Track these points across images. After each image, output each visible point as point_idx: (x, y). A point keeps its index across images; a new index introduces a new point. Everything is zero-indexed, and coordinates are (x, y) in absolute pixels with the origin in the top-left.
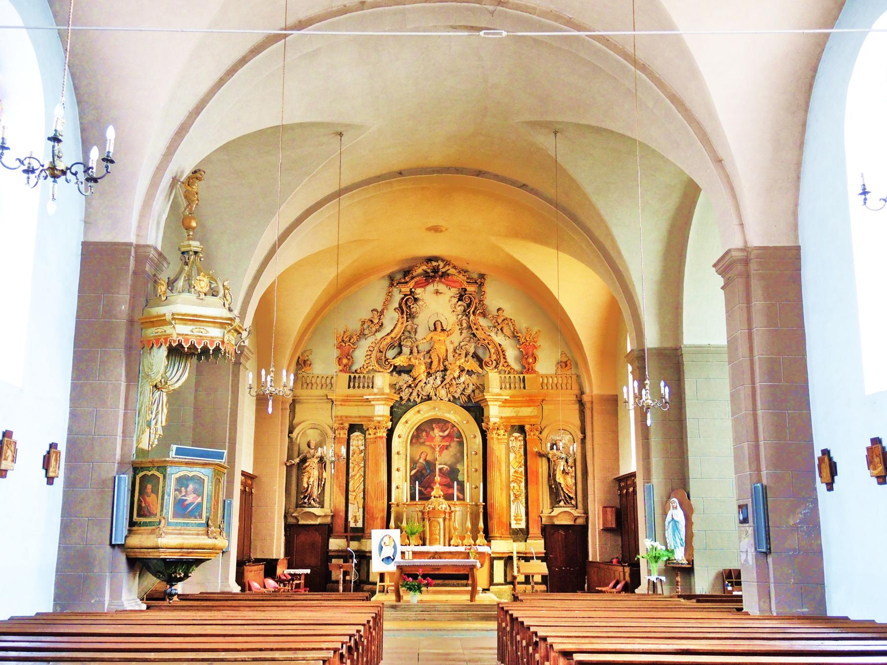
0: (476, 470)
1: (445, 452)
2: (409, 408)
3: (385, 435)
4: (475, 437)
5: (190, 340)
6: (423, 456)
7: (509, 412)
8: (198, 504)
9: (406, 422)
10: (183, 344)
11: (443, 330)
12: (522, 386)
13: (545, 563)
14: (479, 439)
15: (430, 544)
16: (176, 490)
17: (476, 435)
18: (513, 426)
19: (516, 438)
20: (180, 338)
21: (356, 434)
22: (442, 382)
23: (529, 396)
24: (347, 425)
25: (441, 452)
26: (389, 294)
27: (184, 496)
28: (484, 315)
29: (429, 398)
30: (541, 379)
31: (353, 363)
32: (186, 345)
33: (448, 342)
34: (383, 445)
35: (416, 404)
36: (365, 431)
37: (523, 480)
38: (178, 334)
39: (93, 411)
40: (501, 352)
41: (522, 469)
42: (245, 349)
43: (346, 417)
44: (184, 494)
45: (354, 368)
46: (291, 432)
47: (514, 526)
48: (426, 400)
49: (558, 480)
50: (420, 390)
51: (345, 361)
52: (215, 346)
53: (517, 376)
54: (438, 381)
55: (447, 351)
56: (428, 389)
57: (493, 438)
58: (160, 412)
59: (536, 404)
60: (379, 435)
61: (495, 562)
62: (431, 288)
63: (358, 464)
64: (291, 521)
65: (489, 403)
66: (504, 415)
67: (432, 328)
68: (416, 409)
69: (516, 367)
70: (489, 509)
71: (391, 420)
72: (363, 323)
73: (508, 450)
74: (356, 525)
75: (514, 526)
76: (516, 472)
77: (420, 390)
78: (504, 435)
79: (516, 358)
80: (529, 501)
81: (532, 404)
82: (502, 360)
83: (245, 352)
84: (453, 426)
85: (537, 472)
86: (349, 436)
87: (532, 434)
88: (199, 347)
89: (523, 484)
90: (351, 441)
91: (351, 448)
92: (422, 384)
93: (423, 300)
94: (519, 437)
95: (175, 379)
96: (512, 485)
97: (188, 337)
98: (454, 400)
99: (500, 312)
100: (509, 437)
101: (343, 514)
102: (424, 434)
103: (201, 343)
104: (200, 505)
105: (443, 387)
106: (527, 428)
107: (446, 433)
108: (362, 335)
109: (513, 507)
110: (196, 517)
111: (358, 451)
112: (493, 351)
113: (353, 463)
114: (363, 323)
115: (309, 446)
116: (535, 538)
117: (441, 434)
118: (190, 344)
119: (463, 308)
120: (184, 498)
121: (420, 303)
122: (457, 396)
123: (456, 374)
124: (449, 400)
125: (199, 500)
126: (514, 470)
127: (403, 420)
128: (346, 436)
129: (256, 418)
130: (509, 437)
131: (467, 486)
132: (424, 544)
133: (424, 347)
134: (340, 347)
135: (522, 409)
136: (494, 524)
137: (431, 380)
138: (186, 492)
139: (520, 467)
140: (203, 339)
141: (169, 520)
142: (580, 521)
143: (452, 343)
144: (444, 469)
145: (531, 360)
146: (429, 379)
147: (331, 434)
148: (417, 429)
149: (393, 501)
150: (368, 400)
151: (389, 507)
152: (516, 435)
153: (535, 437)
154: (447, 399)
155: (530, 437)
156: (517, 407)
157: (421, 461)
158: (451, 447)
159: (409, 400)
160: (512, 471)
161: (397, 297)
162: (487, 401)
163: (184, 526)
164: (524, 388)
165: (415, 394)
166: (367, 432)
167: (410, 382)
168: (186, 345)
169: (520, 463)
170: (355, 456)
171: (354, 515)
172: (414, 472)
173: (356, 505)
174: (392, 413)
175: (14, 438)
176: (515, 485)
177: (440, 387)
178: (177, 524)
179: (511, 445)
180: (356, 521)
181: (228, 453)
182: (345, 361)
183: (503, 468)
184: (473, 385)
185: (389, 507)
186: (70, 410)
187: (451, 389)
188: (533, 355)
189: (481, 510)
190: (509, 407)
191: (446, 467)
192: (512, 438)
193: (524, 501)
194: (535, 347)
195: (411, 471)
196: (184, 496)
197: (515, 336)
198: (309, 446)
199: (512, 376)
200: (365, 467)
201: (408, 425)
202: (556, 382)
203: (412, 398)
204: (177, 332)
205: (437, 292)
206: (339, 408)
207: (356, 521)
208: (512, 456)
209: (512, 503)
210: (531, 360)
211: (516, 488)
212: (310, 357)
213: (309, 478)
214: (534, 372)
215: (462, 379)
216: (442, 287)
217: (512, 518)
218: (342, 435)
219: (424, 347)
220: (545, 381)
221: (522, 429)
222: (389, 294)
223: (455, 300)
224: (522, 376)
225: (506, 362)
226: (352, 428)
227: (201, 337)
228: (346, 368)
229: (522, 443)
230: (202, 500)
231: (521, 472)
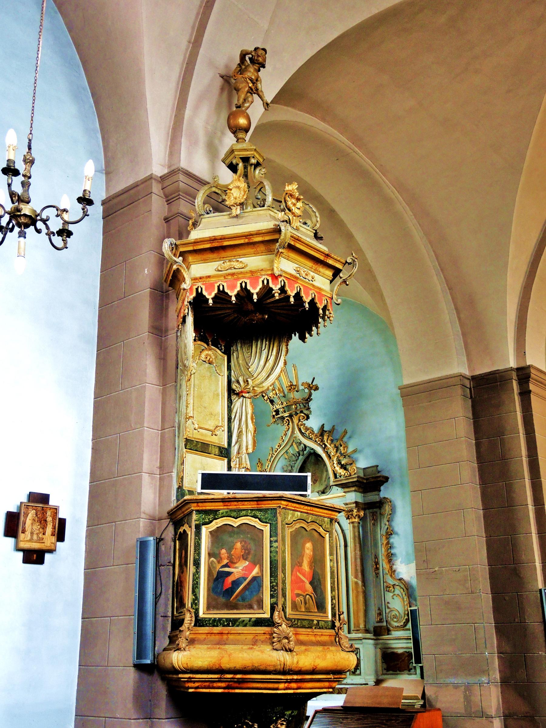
5: (216, 285)
8: (254, 579)
10: (205, 293)
13: (12, 190)
16: (210, 555)
20: (200, 284)
27: (226, 566)
32: (210, 294)
38: (195, 279)
39: (117, 437)
42: (532, 371)
44: (225, 562)
52: (260, 286)
58: (244, 432)
83: (532, 375)
88: (233, 293)
95: (264, 374)
97: (212, 280)
103: (235, 287)
104: (257, 581)
110: (251, 607)
118: (216, 291)
120: (227, 569)
125: (255, 572)
138: (230, 557)
140: (238, 279)
141: (201, 615)
163: (228, 625)
168: (210, 294)
175: (52, 502)
178: (215, 623)
181: (312, 476)
186: (93, 443)
196: (226, 566)
204: (193, 276)
227: (233, 274)
230: (262, 570)
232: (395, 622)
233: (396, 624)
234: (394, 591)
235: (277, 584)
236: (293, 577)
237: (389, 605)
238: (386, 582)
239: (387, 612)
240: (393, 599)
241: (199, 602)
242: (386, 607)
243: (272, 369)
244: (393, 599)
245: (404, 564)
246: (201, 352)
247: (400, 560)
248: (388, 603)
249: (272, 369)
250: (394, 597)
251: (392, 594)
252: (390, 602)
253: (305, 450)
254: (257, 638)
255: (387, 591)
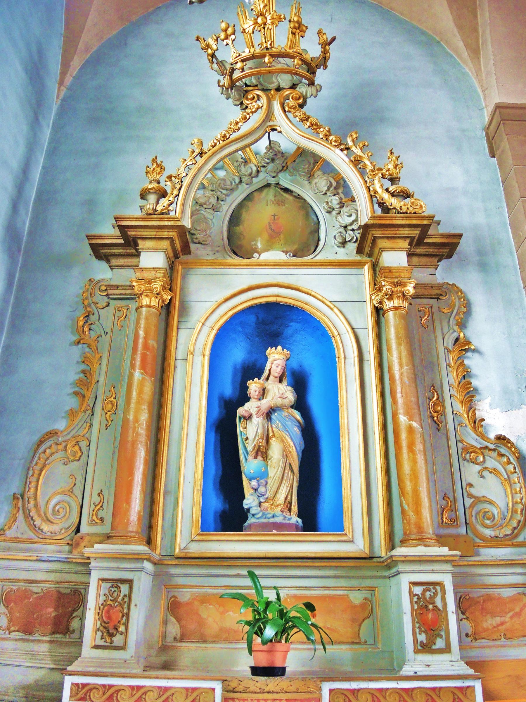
232: (487, 527)
233: (488, 532)
234: (484, 461)
235: (258, 440)
236: (119, 542)
237: (473, 491)
238: (461, 441)
239: (467, 505)
240: (482, 477)
241: (444, 407)
242: (465, 494)
243: (33, 458)
244: (482, 477)
245: (498, 410)
246: (68, 544)
247: (488, 401)
248: (470, 485)
249: (33, 458)
250: (486, 473)
251: (478, 468)
252: (473, 484)
253: (257, 176)
254: (410, 274)
255: (465, 459)
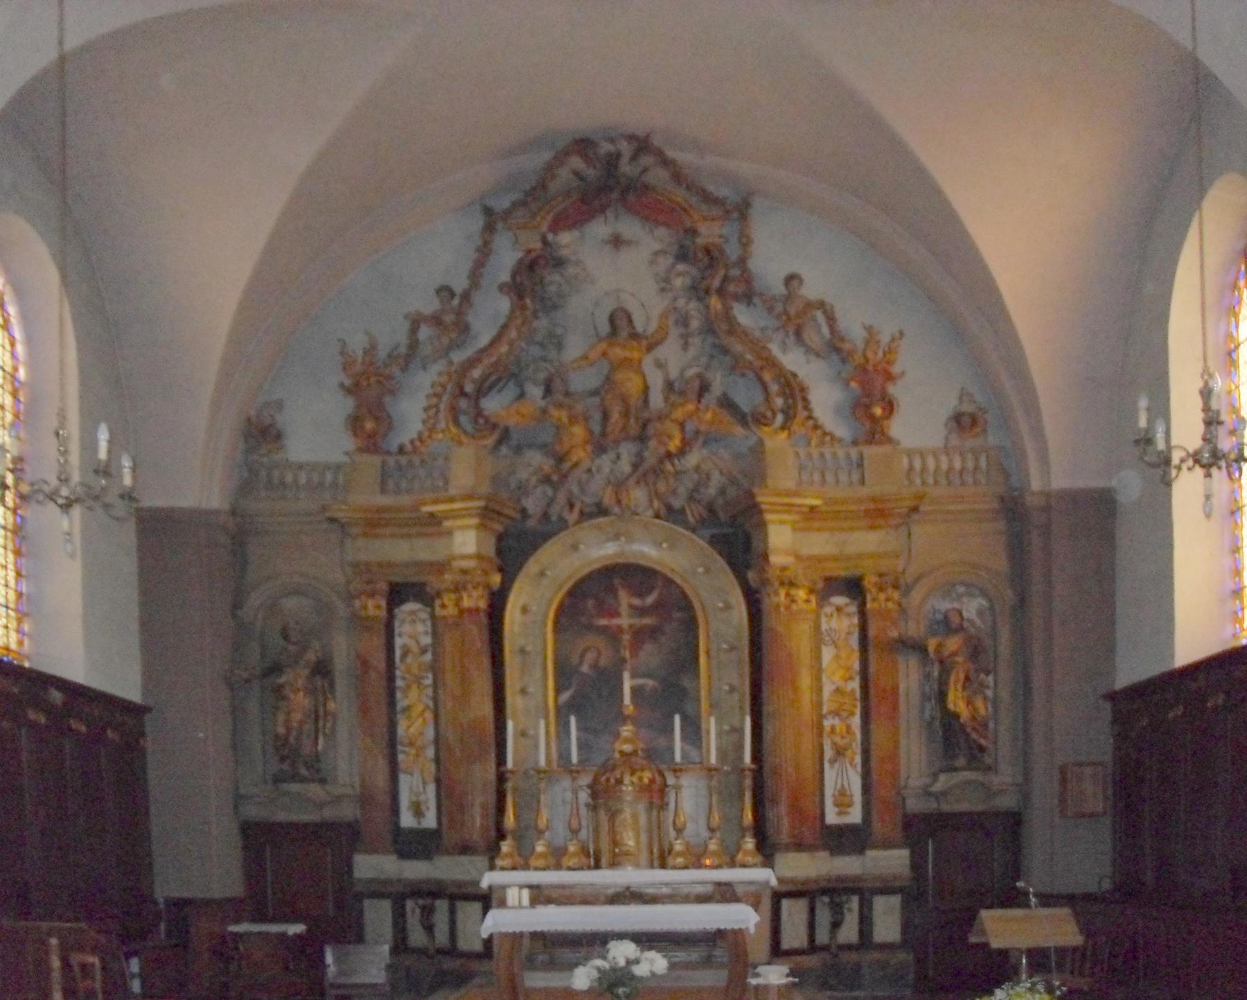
0: (732, 689)
1: (648, 647)
2: (546, 537)
3: (483, 604)
4: (728, 607)
6: (590, 656)
7: (819, 544)
9: (542, 574)
11: (634, 336)
12: (855, 477)
14: (740, 612)
15: (613, 865)
17: (733, 601)
18: (828, 580)
19: (839, 609)
21: (410, 606)
22: (635, 466)
23: (874, 500)
24: (383, 586)
25: (636, 648)
26: (484, 252)
28: (748, 297)
29: (602, 511)
30: (905, 461)
31: (390, 427)
33: (648, 363)
34: (477, 635)
35: (563, 525)
36: (433, 599)
37: (858, 711)
40: (794, 391)
41: (855, 685)
43: (380, 565)
45: (394, 442)
46: (237, 605)
47: (832, 818)
48: (591, 516)
49: (951, 706)
50: (575, 489)
51: (369, 425)
53: (841, 453)
54: (625, 466)
55: (646, 389)
56: (598, 488)
57: (778, 606)
59: (894, 522)
60: (466, 603)
61: (786, 904)
62: (599, 229)
63: (418, 680)
64: (253, 812)
65: (769, 517)
66: (805, 551)
67: (605, 328)
68: (564, 538)
69: (842, 430)
70: (769, 782)
71: (501, 570)
72: (416, 322)
73: (818, 639)
74: (419, 823)
75: (832, 818)
76: (838, 690)
77: (575, 489)
78: (808, 601)
79: (838, 410)
80: (872, 692)
81: (880, 521)
82: (802, 414)
84: (669, 582)
85: (895, 689)
86: (390, 610)
87: (882, 596)
89: (856, 721)
90: (397, 624)
91: (398, 642)
92: (579, 473)
93: (578, 263)
94: (847, 605)
96: (827, 723)
98: (672, 514)
99: (795, 283)
100: (820, 606)
101: (384, 799)
102: (590, 603)
105: (638, 483)
106: (870, 582)
107: (650, 600)
108: (410, 356)
109: (830, 775)
111: (415, 649)
112: (774, 388)
113: (404, 678)
114: (416, 322)
115: (286, 637)
116: (887, 845)
117: (636, 602)
119: (688, 281)
121: (571, 270)
122: (677, 504)
123: (674, 445)
124: (657, 516)
126: (833, 687)
127: (532, 567)
128: (383, 613)
129: (145, 573)
130: (820, 606)
131: (711, 726)
132: (597, 866)
133: (584, 380)
134: (352, 390)
135: (856, 535)
136: (781, 820)
137: (605, 461)
139: (851, 678)
142: (1007, 802)
143: (660, 365)
144: (648, 689)
145: (878, 411)
146: (598, 462)
147: (342, 610)
148: (571, 593)
149: (510, 764)
150: (435, 520)
151: (501, 778)
152: (839, 600)
153: (890, 605)
154: (650, 513)
155: (876, 605)
156: (842, 530)
157: (585, 668)
158: (664, 634)
159: (546, 516)
160: (828, 689)
161: (506, 258)
162: (761, 512)
164: (862, 482)
165: (561, 498)
166: (438, 602)
167: (547, 468)
169: (849, 669)
170: (409, 659)
171: (414, 799)
172: (565, 696)
173: (417, 776)
174: (499, 552)
176: (836, 721)
177: (632, 482)
179: (824, 627)
180: (418, 811)
182: (369, 425)
183: (805, 681)
184: (721, 473)
185: (501, 778)
187: (662, 487)
188: (883, 399)
189: (748, 782)
190: (819, 530)
191: (650, 683)
192: (828, 610)
193: (858, 759)
194: (890, 377)
195: (558, 691)
197: (836, 347)
198: (286, 637)
199: (827, 451)
200: (435, 686)
201: (545, 582)
202: (944, 466)
203: (554, 511)
205: (617, 242)
206: (361, 542)
207: (418, 811)
208: (827, 654)
209: (827, 765)
210: (878, 411)
211: (838, 730)
212: (279, 418)
213: (289, 713)
214: (890, 440)
215: (692, 459)
216: (630, 227)
217: (829, 802)
218: (371, 611)
219: (584, 380)
220: (917, 464)
221: (854, 587)
222: (484, 252)
223: (665, 262)
224: (854, 452)
225: (810, 417)
226: (397, 594)
228: (371, 443)
229: (856, 620)
231: (853, 691)
